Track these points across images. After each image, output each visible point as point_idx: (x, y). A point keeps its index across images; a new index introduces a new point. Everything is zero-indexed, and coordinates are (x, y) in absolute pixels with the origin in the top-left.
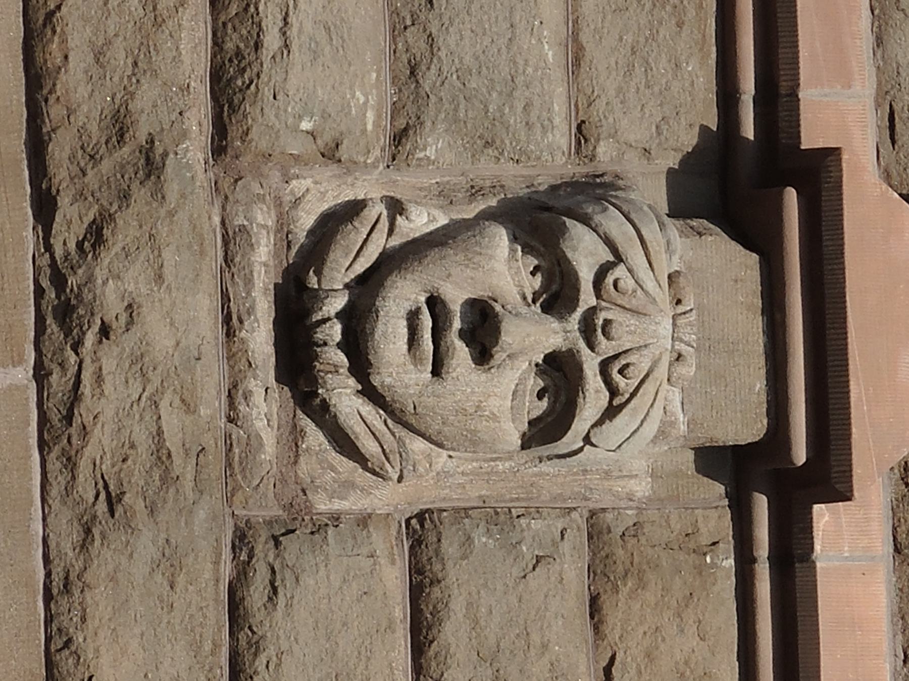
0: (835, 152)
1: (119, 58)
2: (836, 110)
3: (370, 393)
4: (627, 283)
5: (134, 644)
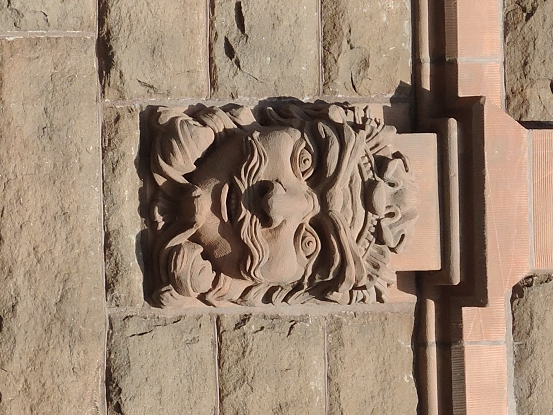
0: (479, 98)
2: (482, 66)
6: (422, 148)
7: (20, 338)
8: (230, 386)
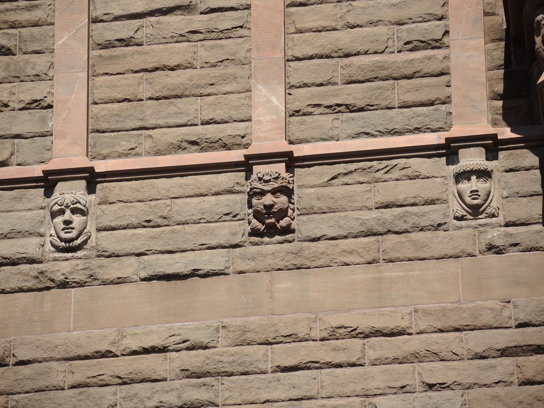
1: (26, 278)
3: (77, 238)
4: (60, 201)
5: (113, 271)
6: (256, 169)
7: (302, 263)
8: (313, 211)
